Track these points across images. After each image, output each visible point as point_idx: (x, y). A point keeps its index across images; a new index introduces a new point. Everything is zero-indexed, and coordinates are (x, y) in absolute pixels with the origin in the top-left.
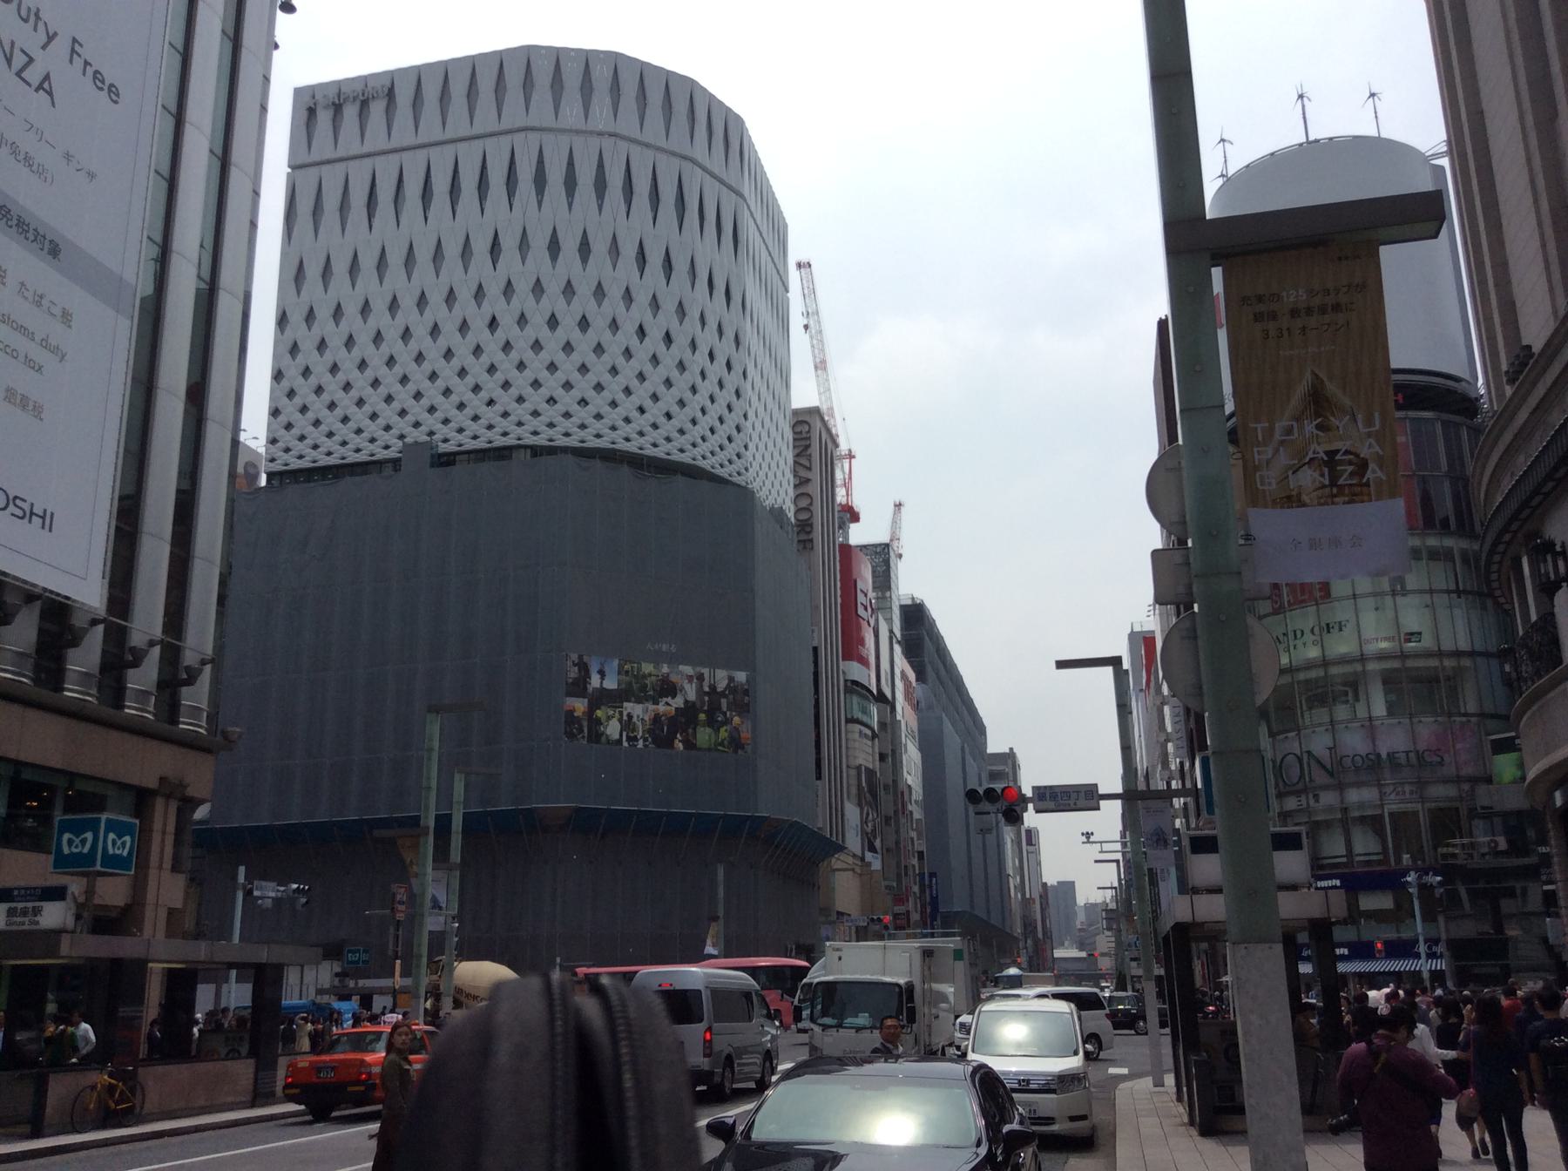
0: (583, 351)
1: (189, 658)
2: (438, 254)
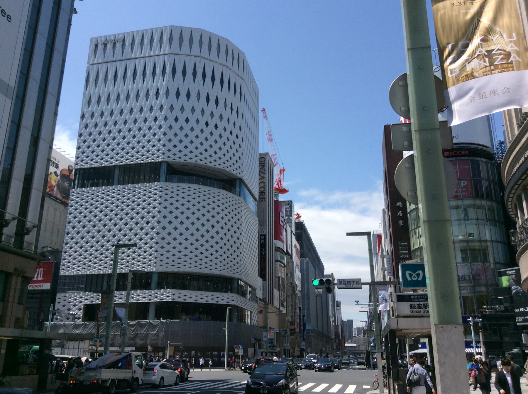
0: (187, 130)
1: (28, 225)
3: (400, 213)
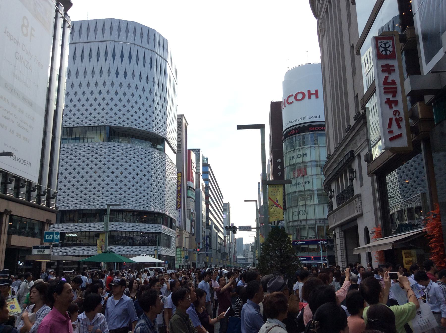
0: (124, 101)
2: (85, 72)
3: (279, 167)
